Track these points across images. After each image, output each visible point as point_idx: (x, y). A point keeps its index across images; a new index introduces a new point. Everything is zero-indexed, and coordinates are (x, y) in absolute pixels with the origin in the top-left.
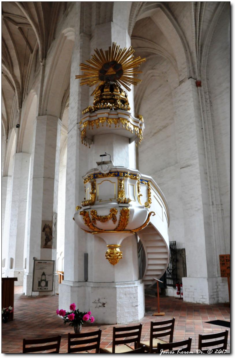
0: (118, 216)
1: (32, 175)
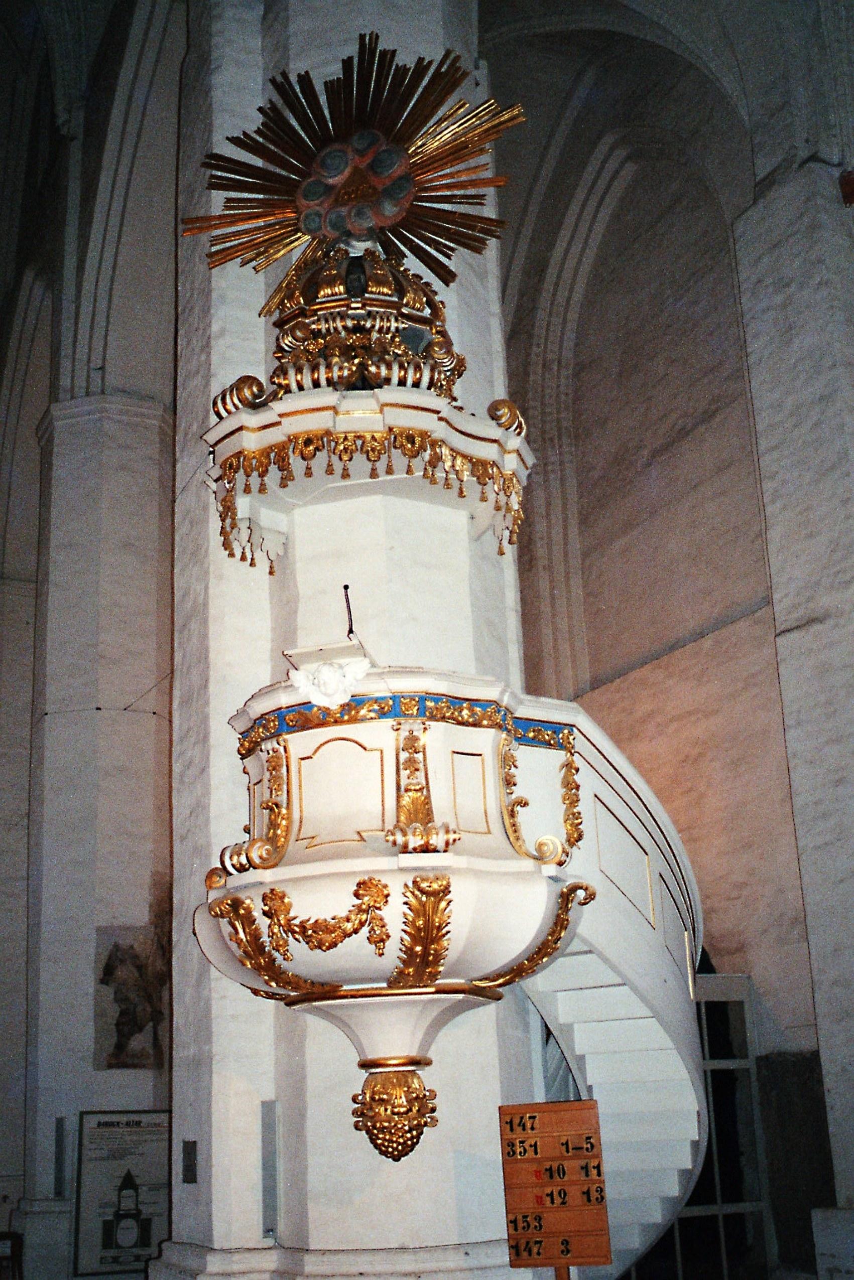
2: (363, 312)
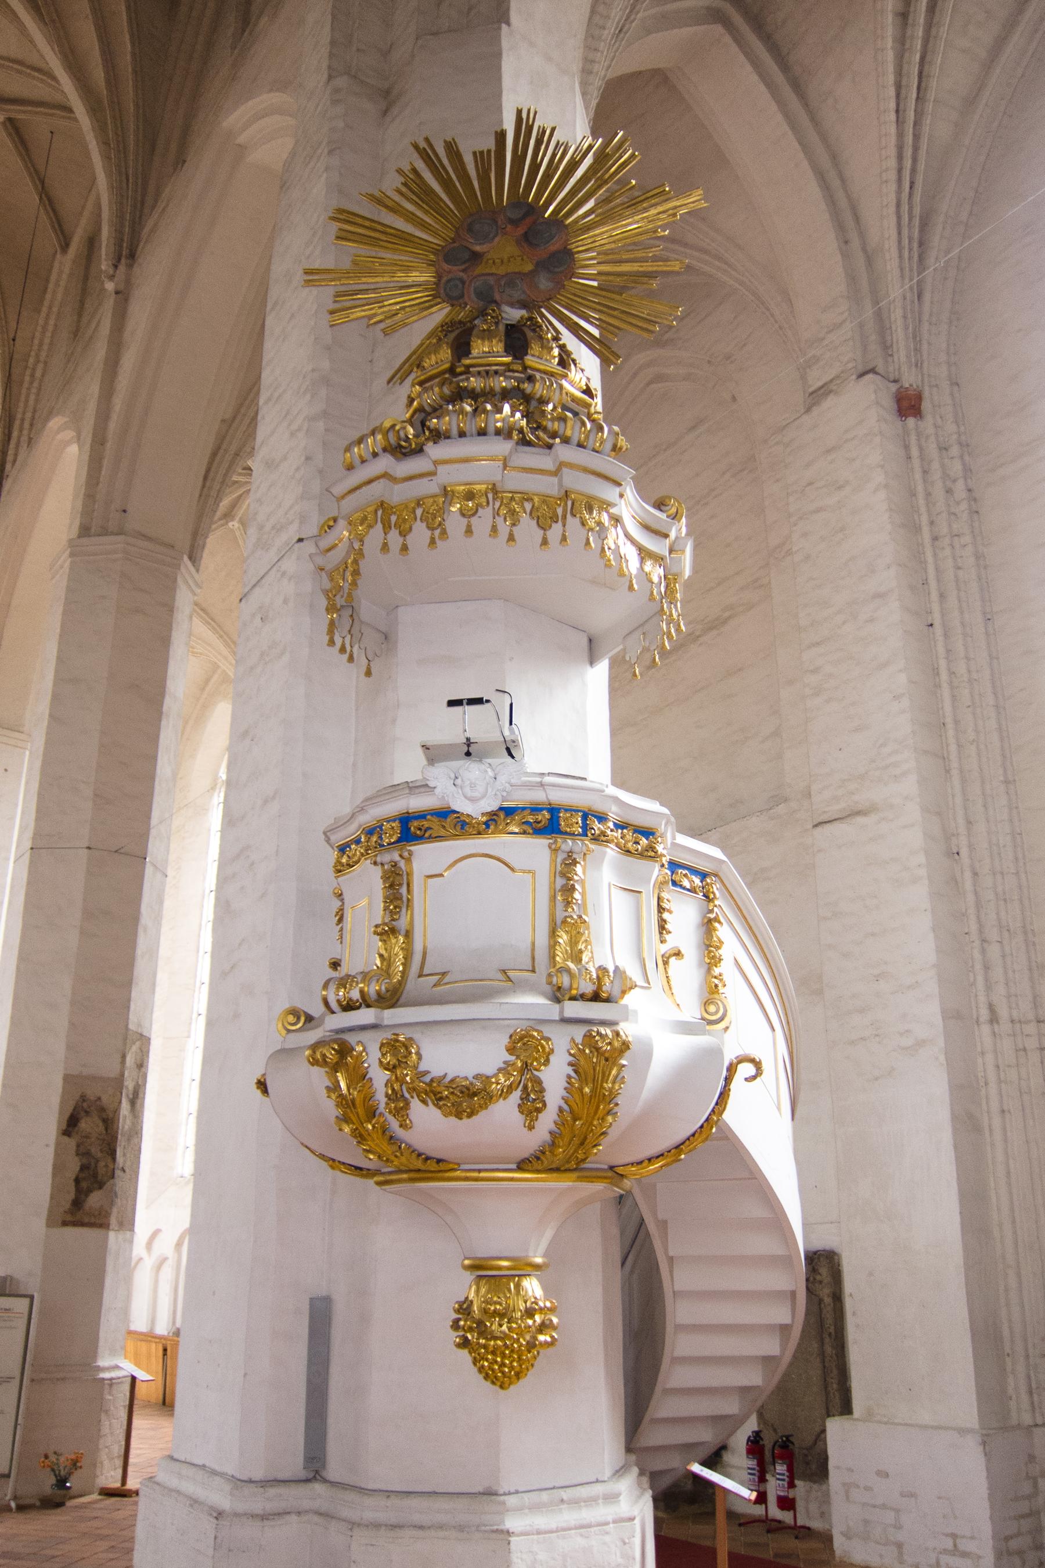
0: (555, 1077)
1: (29, 834)
2: (522, 376)
